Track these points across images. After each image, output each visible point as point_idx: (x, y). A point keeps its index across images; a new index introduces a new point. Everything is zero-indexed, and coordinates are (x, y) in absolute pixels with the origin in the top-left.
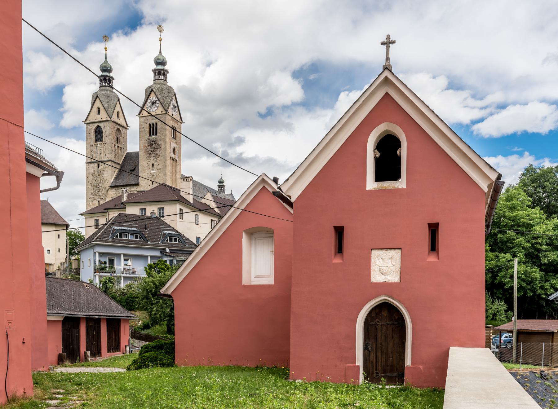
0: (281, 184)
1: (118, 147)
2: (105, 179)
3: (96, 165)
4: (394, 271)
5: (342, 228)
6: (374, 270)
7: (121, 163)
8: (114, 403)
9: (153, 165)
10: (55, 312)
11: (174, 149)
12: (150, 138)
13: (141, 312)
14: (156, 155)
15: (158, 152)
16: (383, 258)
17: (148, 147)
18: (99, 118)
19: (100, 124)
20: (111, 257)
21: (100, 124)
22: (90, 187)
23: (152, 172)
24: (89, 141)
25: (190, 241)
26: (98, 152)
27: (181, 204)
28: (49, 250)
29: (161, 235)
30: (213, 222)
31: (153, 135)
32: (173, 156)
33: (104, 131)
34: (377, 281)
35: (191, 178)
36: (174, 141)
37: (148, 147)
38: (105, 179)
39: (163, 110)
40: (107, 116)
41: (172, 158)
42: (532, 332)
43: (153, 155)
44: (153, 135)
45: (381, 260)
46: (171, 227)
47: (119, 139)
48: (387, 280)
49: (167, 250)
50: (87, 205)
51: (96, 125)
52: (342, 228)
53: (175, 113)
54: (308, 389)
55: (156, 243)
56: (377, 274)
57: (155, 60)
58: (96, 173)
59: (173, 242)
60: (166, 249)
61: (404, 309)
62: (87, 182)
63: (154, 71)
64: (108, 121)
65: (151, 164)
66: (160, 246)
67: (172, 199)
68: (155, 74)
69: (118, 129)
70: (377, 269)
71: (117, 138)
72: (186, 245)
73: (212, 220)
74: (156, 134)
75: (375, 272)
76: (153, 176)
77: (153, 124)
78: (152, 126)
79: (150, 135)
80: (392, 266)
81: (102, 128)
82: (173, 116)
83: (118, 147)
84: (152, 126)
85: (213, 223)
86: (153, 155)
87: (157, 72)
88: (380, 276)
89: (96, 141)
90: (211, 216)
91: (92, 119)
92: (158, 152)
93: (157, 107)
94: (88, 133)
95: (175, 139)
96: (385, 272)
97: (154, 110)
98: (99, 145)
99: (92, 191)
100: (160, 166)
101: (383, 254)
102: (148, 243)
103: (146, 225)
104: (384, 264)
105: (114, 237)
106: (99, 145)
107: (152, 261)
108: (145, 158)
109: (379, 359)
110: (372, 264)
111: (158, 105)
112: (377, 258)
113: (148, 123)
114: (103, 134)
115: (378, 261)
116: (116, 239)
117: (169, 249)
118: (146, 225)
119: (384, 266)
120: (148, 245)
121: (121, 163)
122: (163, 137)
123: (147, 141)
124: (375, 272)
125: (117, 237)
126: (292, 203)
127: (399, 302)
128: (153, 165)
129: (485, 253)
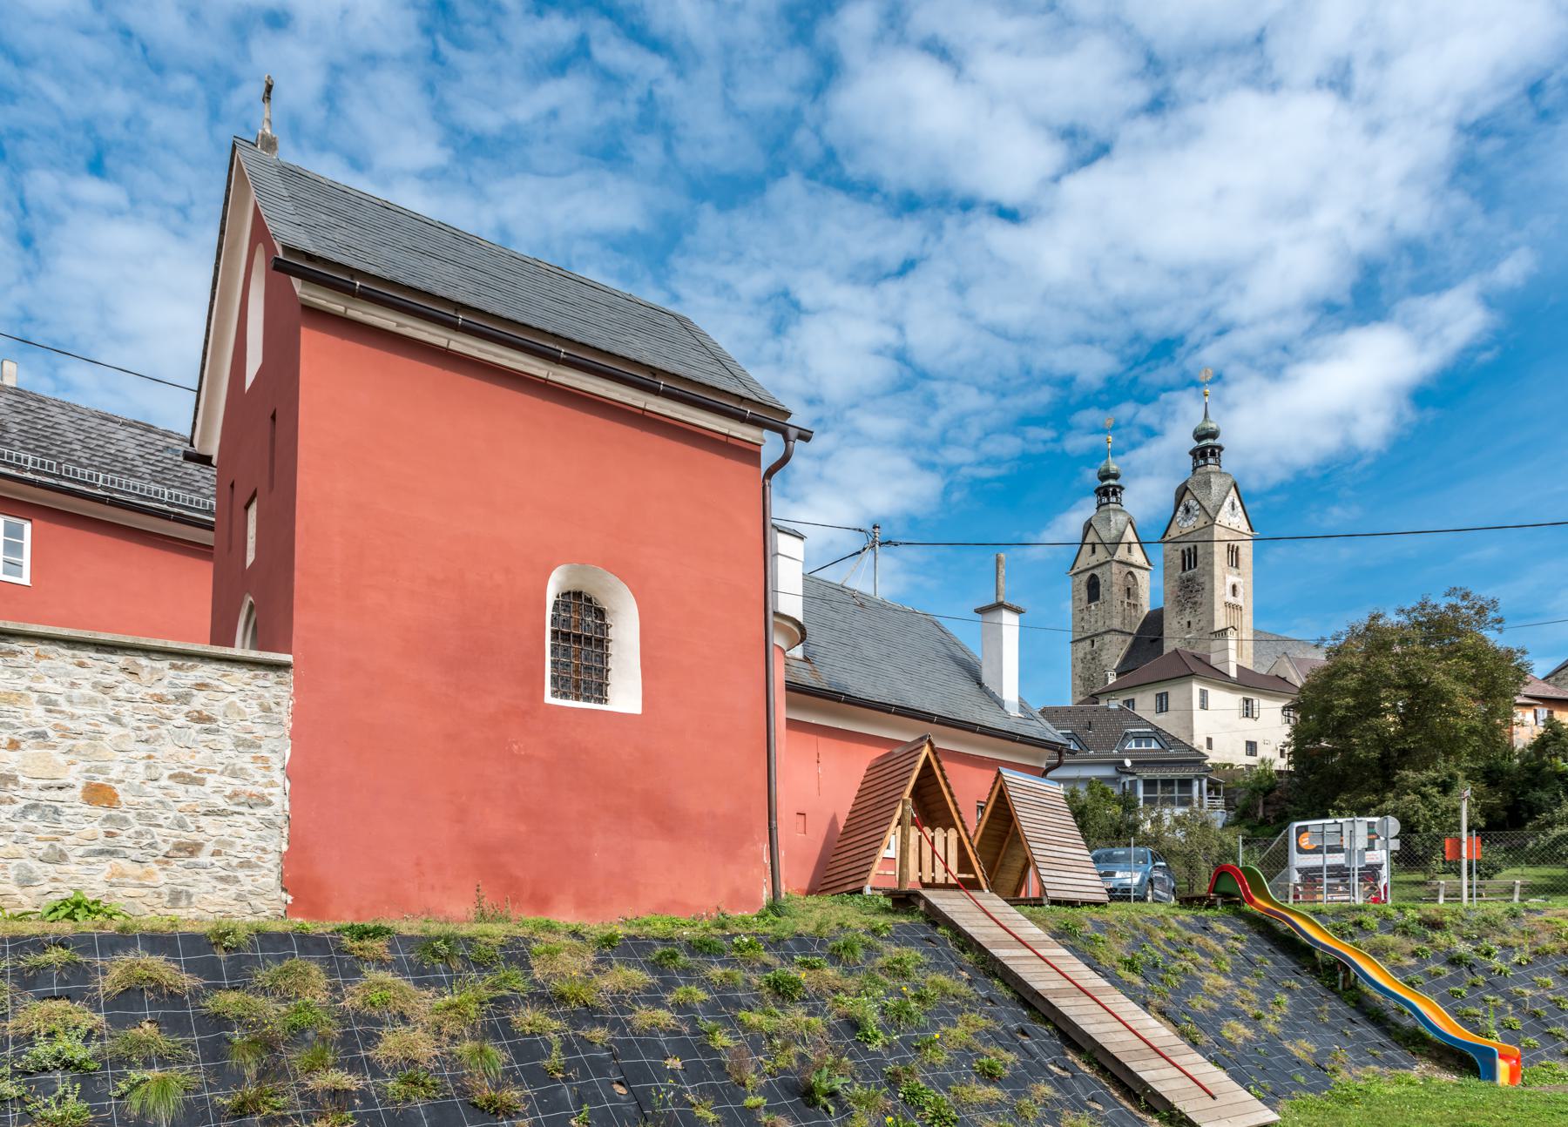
1: (1129, 604)
2: (1103, 663)
3: (1089, 642)
7: (213, 450)
9: (1189, 623)
11: (1234, 587)
12: (1184, 575)
13: (252, 673)
14: (1195, 603)
15: (1198, 599)
17: (1179, 594)
18: (1093, 561)
19: (1096, 572)
21: (1096, 572)
22: (1078, 682)
23: (1188, 636)
24: (1077, 604)
26: (1092, 620)
27: (1205, 681)
30: (1250, 703)
31: (1190, 568)
32: (1231, 599)
33: (1101, 581)
35: (1232, 629)
36: (1235, 571)
37: (1179, 594)
38: (1103, 663)
39: (1207, 519)
40: (1106, 554)
41: (1228, 605)
43: (1190, 605)
44: (1190, 568)
47: (1131, 591)
49: (1128, 763)
51: (1088, 575)
53: (1236, 520)
55: (1106, 752)
57: (1195, 433)
58: (1089, 657)
62: (1074, 674)
63: (1193, 453)
64: (1108, 562)
65: (1184, 622)
67: (1182, 674)
68: (1195, 458)
69: (1131, 573)
71: (1129, 589)
73: (1247, 701)
74: (1195, 565)
76: (1189, 643)
77: (1189, 549)
78: (1186, 552)
79: (1184, 570)
81: (1099, 576)
82: (1231, 527)
83: (1129, 604)
84: (1186, 552)
85: (1250, 706)
86: (1190, 605)
87: (1198, 453)
89: (1089, 602)
90: (1243, 690)
91: (1081, 565)
92: (1198, 599)
93: (1197, 516)
94: (1075, 590)
95: (1237, 566)
97: (1191, 523)
98: (1093, 607)
99: (1082, 689)
100: (1202, 624)
106: (1093, 607)
108: (1174, 614)
111: (1197, 513)
113: (1180, 549)
114: (1101, 588)
121: (213, 450)
122: (1208, 568)
123: (1178, 583)
128: (1189, 623)
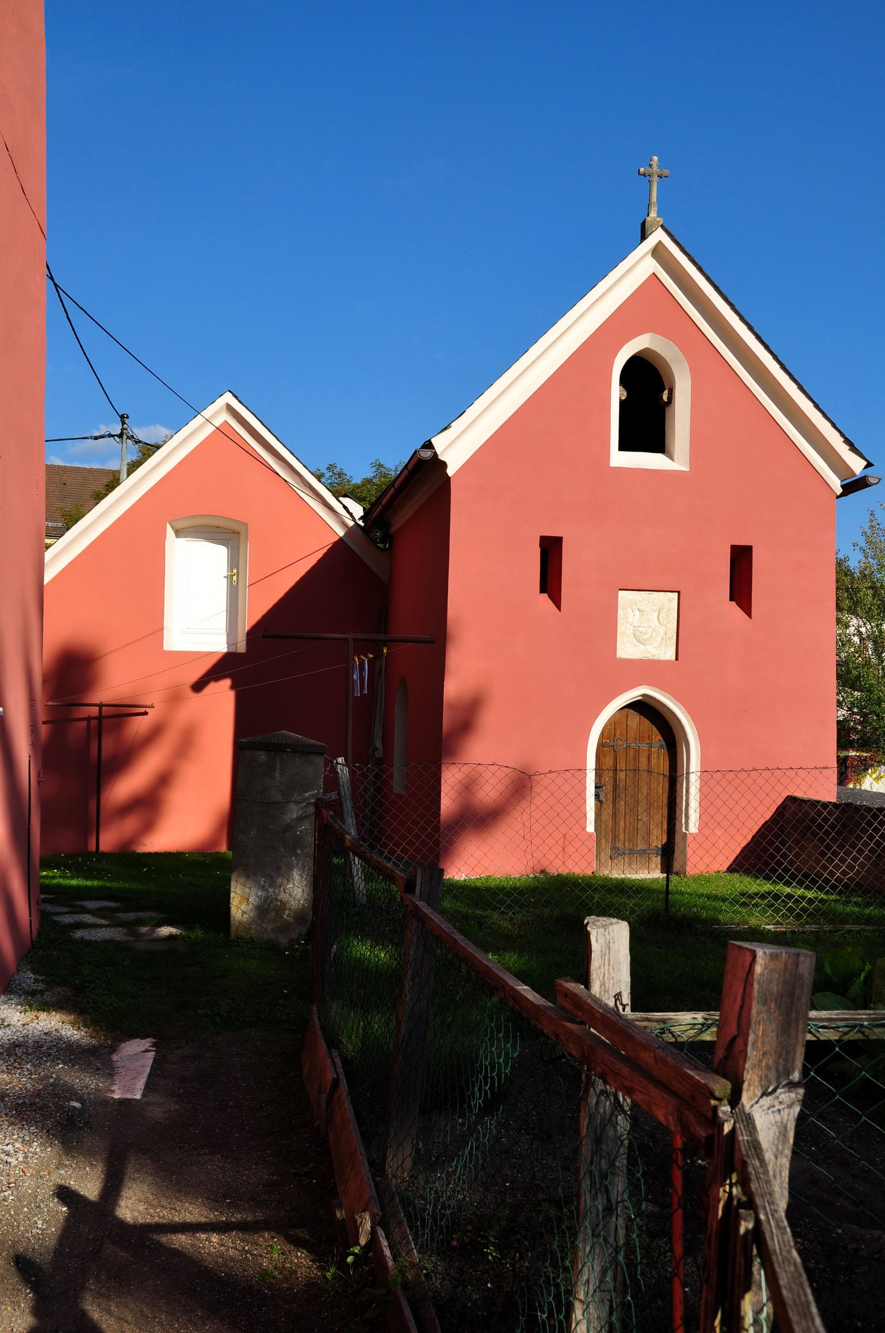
0: (112, 438)
4: (664, 636)
5: (558, 541)
6: (623, 633)
8: (177, 1110)
10: (626, 811)
16: (642, 608)
28: (239, 533)
34: (628, 657)
45: (637, 613)
48: (649, 656)
52: (558, 541)
56: (629, 642)
61: (685, 716)
70: (630, 631)
75: (626, 637)
80: (660, 626)
88: (636, 646)
96: (645, 637)
101: (641, 602)
104: (643, 621)
109: (621, 829)
110: (620, 621)
112: (630, 609)
115: (631, 614)
119: (643, 625)
124: (626, 637)
126: (450, 478)
127: (679, 699)
129: (834, 613)
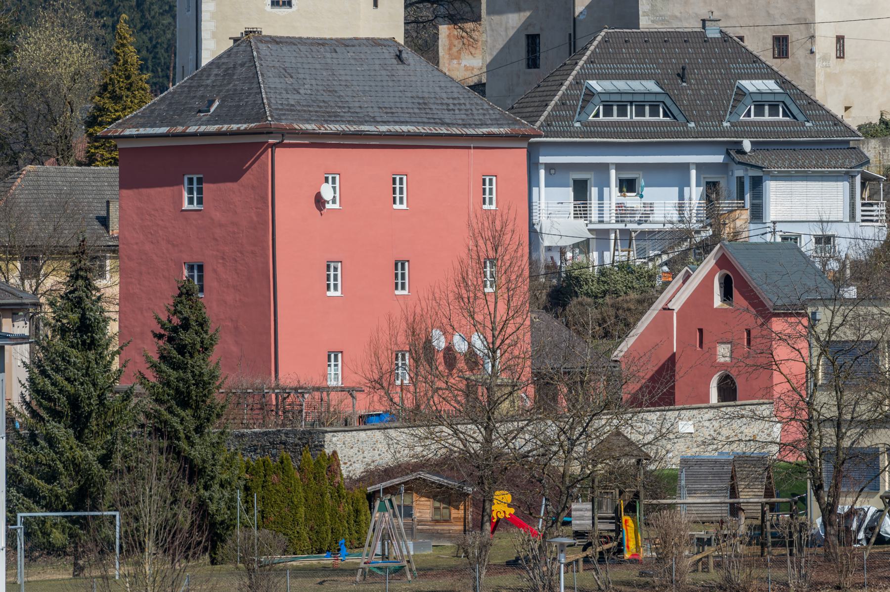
20: (334, 176)
25: (821, 107)
29: (731, 95)
42: (746, 282)
46: (762, 63)
49: (747, 145)
50: (405, 23)
54: (259, 406)
59: (647, 118)
60: (741, 142)
66: (723, 133)
72: (807, 124)
102: (687, 126)
103: (683, 69)
105: (741, 118)
107: (702, 176)
116: (594, 124)
117: (751, 142)
118: (683, 69)
120: (687, 134)
125: (597, 115)
